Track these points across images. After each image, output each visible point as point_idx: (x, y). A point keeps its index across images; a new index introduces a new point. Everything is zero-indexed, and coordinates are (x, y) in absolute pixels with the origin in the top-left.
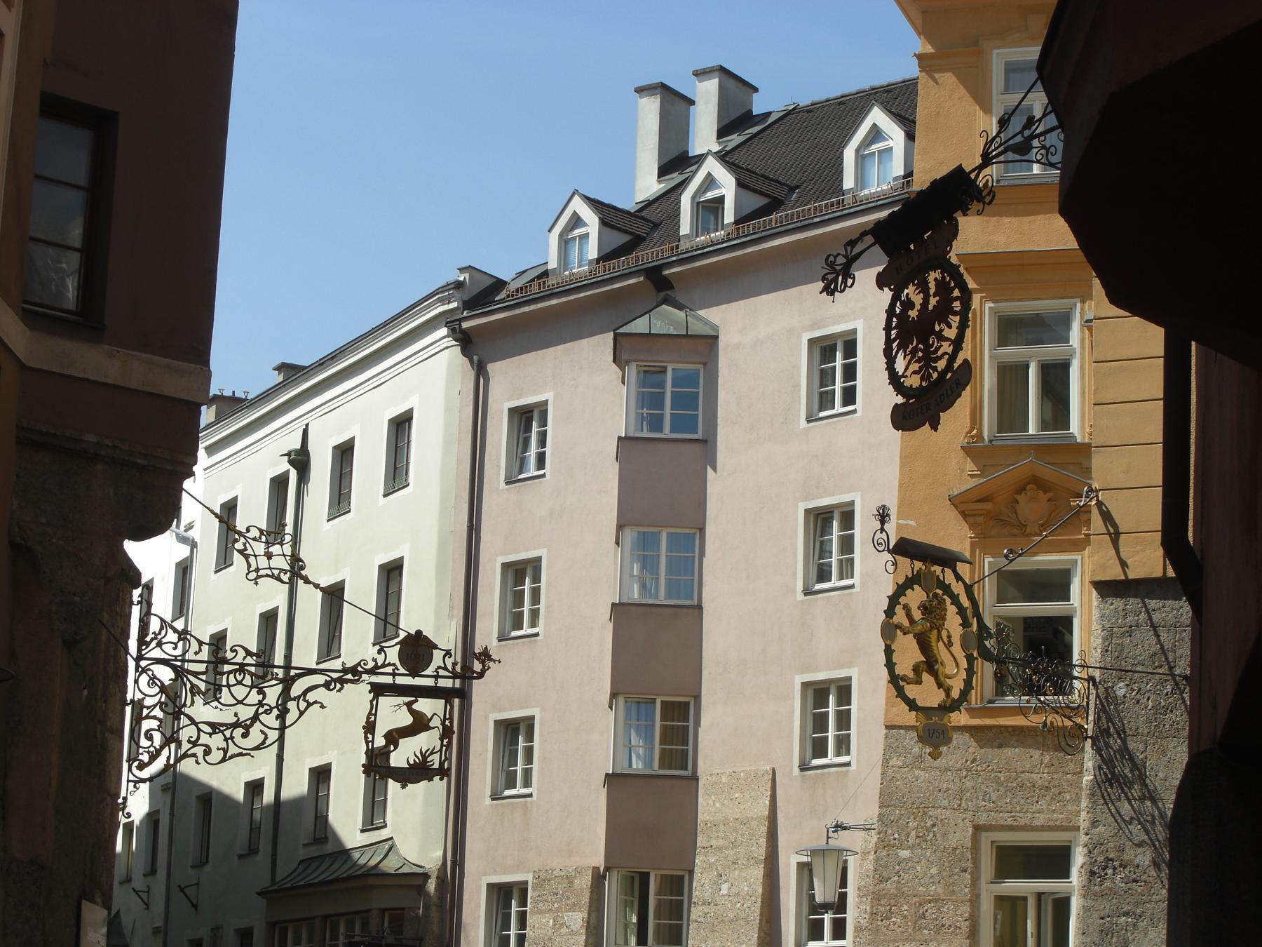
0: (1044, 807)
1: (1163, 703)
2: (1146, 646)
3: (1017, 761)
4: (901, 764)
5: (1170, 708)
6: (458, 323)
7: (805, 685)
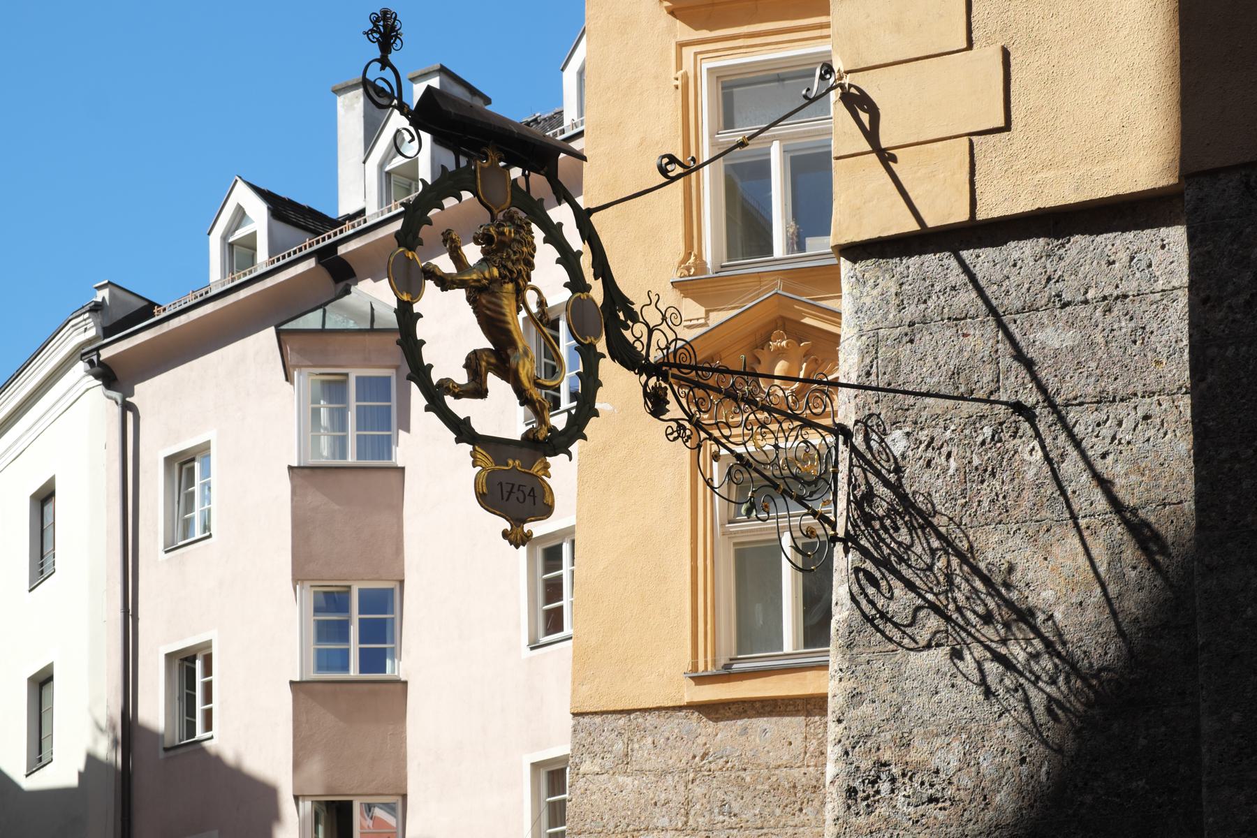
0: (811, 817)
1: (976, 462)
2: (942, 358)
3: (768, 752)
4: (597, 769)
5: (990, 469)
6: (95, 353)
7: (536, 766)
